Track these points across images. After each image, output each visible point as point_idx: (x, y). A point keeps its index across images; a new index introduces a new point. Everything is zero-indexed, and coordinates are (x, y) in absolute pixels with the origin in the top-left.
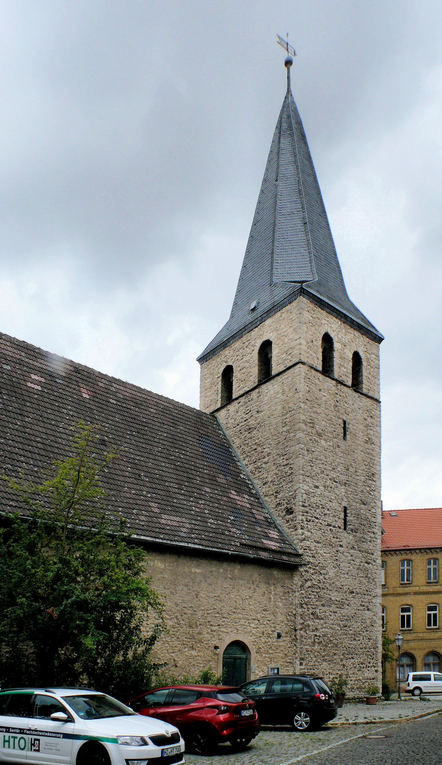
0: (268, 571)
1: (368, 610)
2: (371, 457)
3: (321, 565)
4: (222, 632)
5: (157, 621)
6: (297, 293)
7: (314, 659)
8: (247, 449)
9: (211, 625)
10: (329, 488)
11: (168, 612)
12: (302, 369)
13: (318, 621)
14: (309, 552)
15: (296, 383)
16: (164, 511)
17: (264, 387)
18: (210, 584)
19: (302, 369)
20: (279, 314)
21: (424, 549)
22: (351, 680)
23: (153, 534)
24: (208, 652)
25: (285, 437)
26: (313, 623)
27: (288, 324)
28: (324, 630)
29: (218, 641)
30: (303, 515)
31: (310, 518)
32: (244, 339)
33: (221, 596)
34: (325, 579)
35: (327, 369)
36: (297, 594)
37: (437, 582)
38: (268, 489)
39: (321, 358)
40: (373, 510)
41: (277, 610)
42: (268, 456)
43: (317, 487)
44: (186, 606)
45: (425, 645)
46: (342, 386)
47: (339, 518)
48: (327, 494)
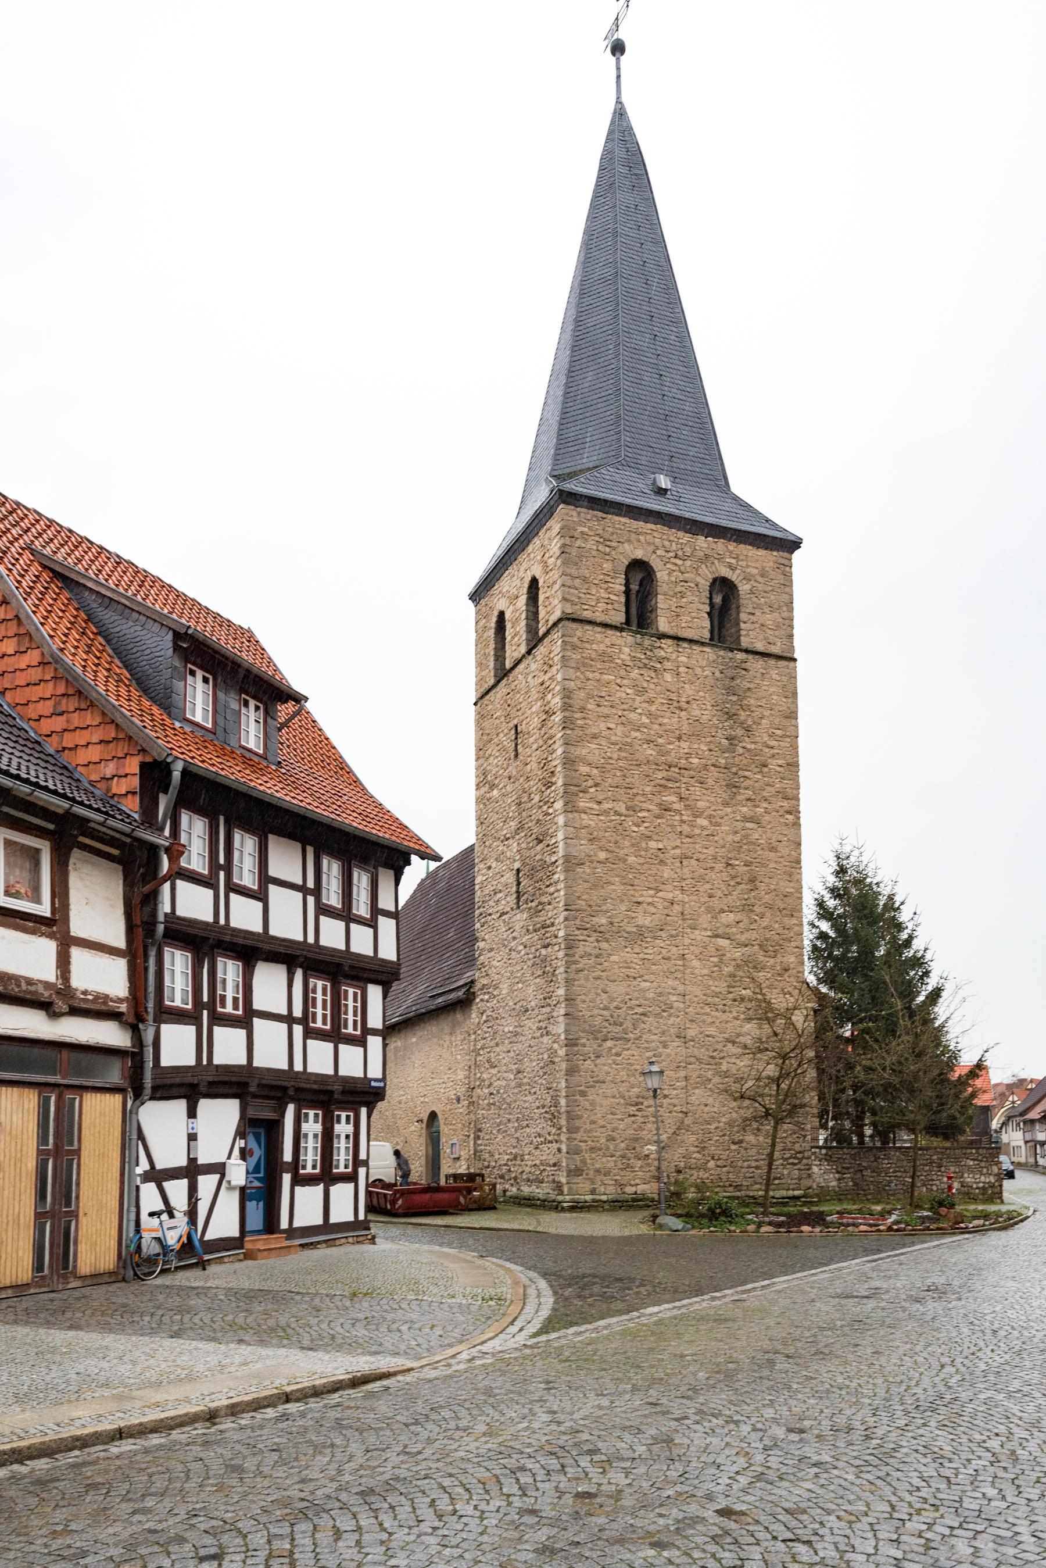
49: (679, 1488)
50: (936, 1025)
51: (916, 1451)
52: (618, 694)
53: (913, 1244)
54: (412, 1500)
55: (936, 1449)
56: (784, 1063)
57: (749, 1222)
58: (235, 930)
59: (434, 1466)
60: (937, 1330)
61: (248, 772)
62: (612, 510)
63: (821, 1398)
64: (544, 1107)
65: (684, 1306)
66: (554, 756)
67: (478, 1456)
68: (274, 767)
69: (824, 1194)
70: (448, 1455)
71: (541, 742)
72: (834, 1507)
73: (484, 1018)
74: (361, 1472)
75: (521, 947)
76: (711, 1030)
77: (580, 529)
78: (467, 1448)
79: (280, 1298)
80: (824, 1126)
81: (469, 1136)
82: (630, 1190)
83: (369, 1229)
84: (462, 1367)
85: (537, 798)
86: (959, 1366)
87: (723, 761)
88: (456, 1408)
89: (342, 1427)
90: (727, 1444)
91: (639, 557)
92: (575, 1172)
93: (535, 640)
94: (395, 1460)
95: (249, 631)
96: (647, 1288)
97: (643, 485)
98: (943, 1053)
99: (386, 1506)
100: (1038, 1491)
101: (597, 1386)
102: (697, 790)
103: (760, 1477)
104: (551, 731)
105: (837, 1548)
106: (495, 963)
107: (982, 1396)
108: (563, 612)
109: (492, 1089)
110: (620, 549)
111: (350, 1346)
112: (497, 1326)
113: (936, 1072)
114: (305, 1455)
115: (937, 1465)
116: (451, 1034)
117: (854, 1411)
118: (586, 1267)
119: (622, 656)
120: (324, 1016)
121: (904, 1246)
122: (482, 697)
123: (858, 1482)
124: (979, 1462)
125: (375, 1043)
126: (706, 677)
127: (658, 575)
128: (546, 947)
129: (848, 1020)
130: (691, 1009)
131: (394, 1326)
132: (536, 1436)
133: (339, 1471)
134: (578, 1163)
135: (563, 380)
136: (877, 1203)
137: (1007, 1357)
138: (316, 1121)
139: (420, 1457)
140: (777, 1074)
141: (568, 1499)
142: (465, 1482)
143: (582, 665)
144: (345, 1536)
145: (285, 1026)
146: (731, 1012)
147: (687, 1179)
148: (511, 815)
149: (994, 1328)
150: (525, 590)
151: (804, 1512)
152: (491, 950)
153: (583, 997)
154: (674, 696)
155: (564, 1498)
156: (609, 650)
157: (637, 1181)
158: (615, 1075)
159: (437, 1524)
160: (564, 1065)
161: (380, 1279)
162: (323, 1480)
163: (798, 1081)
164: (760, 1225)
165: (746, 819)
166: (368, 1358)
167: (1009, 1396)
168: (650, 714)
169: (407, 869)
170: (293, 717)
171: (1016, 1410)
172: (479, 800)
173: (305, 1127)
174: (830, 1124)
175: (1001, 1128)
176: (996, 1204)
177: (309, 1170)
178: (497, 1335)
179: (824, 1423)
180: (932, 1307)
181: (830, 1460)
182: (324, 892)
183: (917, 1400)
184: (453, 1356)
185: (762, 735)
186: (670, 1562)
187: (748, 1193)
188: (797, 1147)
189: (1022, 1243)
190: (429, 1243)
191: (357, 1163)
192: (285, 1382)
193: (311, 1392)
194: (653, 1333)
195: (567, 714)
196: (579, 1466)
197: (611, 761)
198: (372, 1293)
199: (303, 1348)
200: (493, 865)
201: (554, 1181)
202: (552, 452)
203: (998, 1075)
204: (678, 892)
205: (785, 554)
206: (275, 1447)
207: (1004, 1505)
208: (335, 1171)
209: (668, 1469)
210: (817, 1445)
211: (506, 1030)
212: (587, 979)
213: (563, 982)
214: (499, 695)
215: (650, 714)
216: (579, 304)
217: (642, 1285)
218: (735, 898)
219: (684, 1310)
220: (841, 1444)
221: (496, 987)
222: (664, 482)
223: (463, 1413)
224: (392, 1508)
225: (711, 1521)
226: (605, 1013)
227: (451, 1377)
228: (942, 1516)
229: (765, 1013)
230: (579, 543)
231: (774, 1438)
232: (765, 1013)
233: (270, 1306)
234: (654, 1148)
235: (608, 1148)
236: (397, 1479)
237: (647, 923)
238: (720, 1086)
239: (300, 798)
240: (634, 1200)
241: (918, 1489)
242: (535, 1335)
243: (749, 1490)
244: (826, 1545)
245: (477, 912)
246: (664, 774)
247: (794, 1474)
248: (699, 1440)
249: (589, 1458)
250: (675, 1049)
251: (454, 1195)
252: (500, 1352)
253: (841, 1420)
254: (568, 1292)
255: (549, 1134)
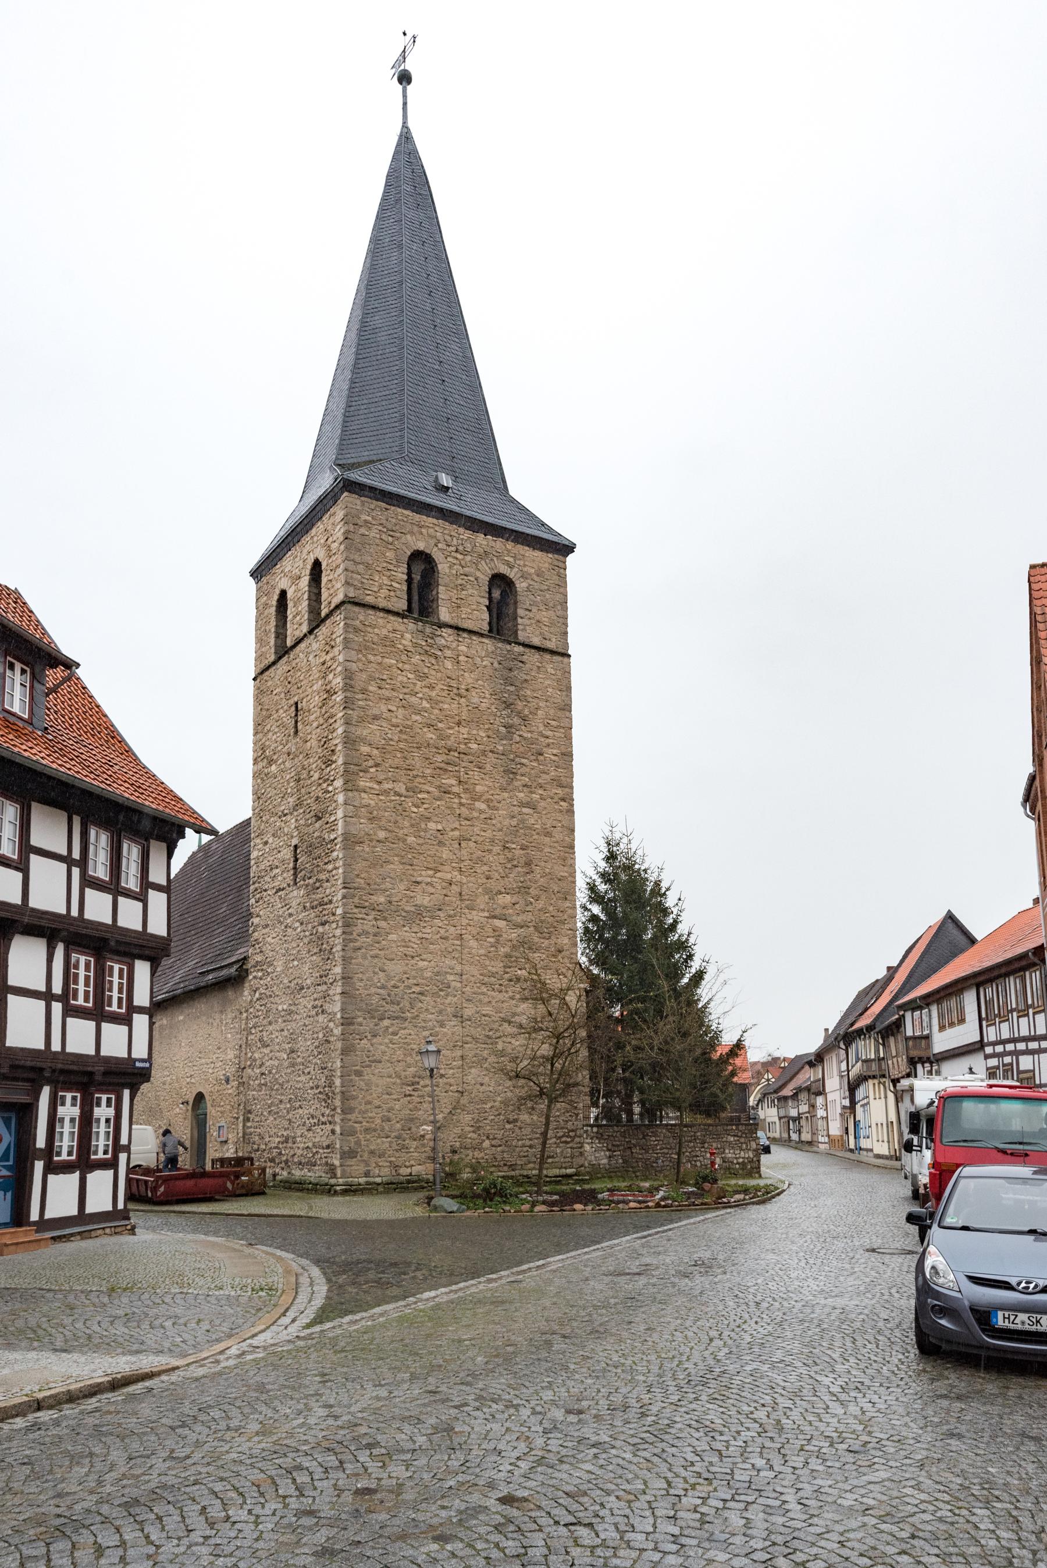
49: (461, 1478)
50: (700, 1006)
51: (689, 1426)
52: (400, 678)
53: (680, 1220)
54: (181, 1509)
55: (708, 1423)
56: (558, 1042)
57: (524, 1202)
58: (33, 910)
59: (204, 1470)
60: (705, 1304)
61: (11, 737)
63: (598, 1377)
64: (317, 1087)
65: (461, 1289)
66: (335, 735)
67: (251, 1457)
68: (40, 733)
69: (595, 1173)
70: (219, 1458)
71: (321, 721)
72: (614, 1487)
73: (257, 995)
74: (125, 1482)
75: (297, 924)
76: (487, 1010)
77: (364, 517)
78: (240, 1449)
79: (29, 1296)
80: (595, 1104)
81: (237, 1119)
82: (405, 1171)
83: (129, 1219)
84: (231, 1362)
85: (316, 776)
86: (726, 1338)
87: (501, 748)
88: (226, 1407)
89: (102, 1434)
90: (508, 1429)
91: (422, 548)
92: (349, 1154)
93: (317, 621)
94: (161, 1466)
95: (16, 591)
96: (424, 1272)
97: (427, 482)
98: (706, 1033)
99: (153, 1517)
100: (802, 1459)
101: (374, 1377)
102: (476, 775)
103: (541, 1461)
104: (331, 710)
105: (617, 1528)
106: (269, 939)
107: (748, 1368)
108: (346, 596)
109: (263, 1069)
110: (403, 540)
111: (109, 1346)
112: (268, 1319)
113: (699, 1051)
114: (61, 1467)
115: (709, 1439)
116: (221, 1012)
117: (629, 1388)
118: (361, 1252)
119: (404, 642)
120: (87, 993)
121: (672, 1222)
122: (262, 673)
123: (635, 1460)
124: (748, 1433)
125: (141, 1022)
126: (485, 667)
127: (440, 567)
128: (323, 924)
129: (619, 1000)
130: (468, 988)
131: (157, 1323)
132: (313, 1432)
133: (100, 1483)
134: (352, 1145)
135: (348, 375)
136: (646, 1180)
137: (770, 1328)
138: (74, 1105)
139: (189, 1461)
140: (551, 1053)
141: (347, 1497)
142: (238, 1485)
143: (365, 648)
144: (108, 1552)
145: (42, 1004)
146: (507, 992)
147: (462, 1159)
148: (289, 790)
149: (757, 1300)
150: (308, 572)
151: (585, 1494)
152: (267, 926)
153: (360, 975)
154: (454, 684)
155: (343, 1495)
156: (391, 635)
157: (412, 1162)
158: (391, 1054)
159: (208, 1533)
160: (339, 1045)
161: (142, 1272)
162: (81, 1493)
163: (572, 1060)
164: (534, 1204)
165: (522, 805)
166: (129, 1358)
167: (773, 1367)
168: (430, 699)
169: (181, 842)
170: (62, 683)
171: (779, 1379)
172: (256, 775)
173: (61, 1111)
174: (602, 1101)
175: (757, 1105)
176: (755, 1178)
177: (64, 1156)
178: (268, 1328)
179: (601, 1402)
180: (699, 1281)
181: (608, 1439)
182: (91, 863)
183: (689, 1375)
184: (222, 1352)
185: (537, 724)
186: (454, 1555)
187: (522, 1172)
188: (569, 1125)
189: (779, 1216)
190: (195, 1231)
191: (117, 1148)
192: (36, 1388)
193: (81, 1395)
194: (430, 1319)
195: (348, 694)
196: (358, 1461)
197: (391, 743)
198: (132, 1288)
199: (56, 1350)
200: (270, 841)
201: (327, 1163)
202: (337, 441)
203: (755, 1054)
204: (456, 873)
205: (561, 558)
206: (26, 1460)
207: (772, 1474)
208: (93, 1157)
209: (449, 1459)
210: (595, 1425)
211: (280, 1008)
212: (365, 957)
213: (340, 960)
214: (279, 672)
215: (430, 699)
216: (364, 306)
217: (417, 1269)
218: (513, 880)
219: (460, 1294)
220: (618, 1423)
221: (270, 964)
222: (445, 480)
223: (234, 1412)
224: (160, 1518)
225: (494, 1510)
226: (382, 991)
227: (220, 1374)
228: (715, 1490)
229: (540, 993)
230: (363, 531)
231: (554, 1421)
232: (540, 993)
233: (18, 1305)
234: (430, 1128)
235: (383, 1130)
236: (164, 1487)
237: (425, 902)
238: (496, 1065)
239: (68, 766)
240: (409, 1182)
241: (692, 1464)
242: (308, 1326)
243: (531, 1476)
244: (607, 1526)
245: (252, 888)
246: (444, 757)
247: (573, 1456)
248: (479, 1427)
249: (368, 1452)
250: (452, 1028)
251: (220, 1181)
252: (272, 1345)
253: (617, 1399)
254: (342, 1279)
255: (323, 1115)
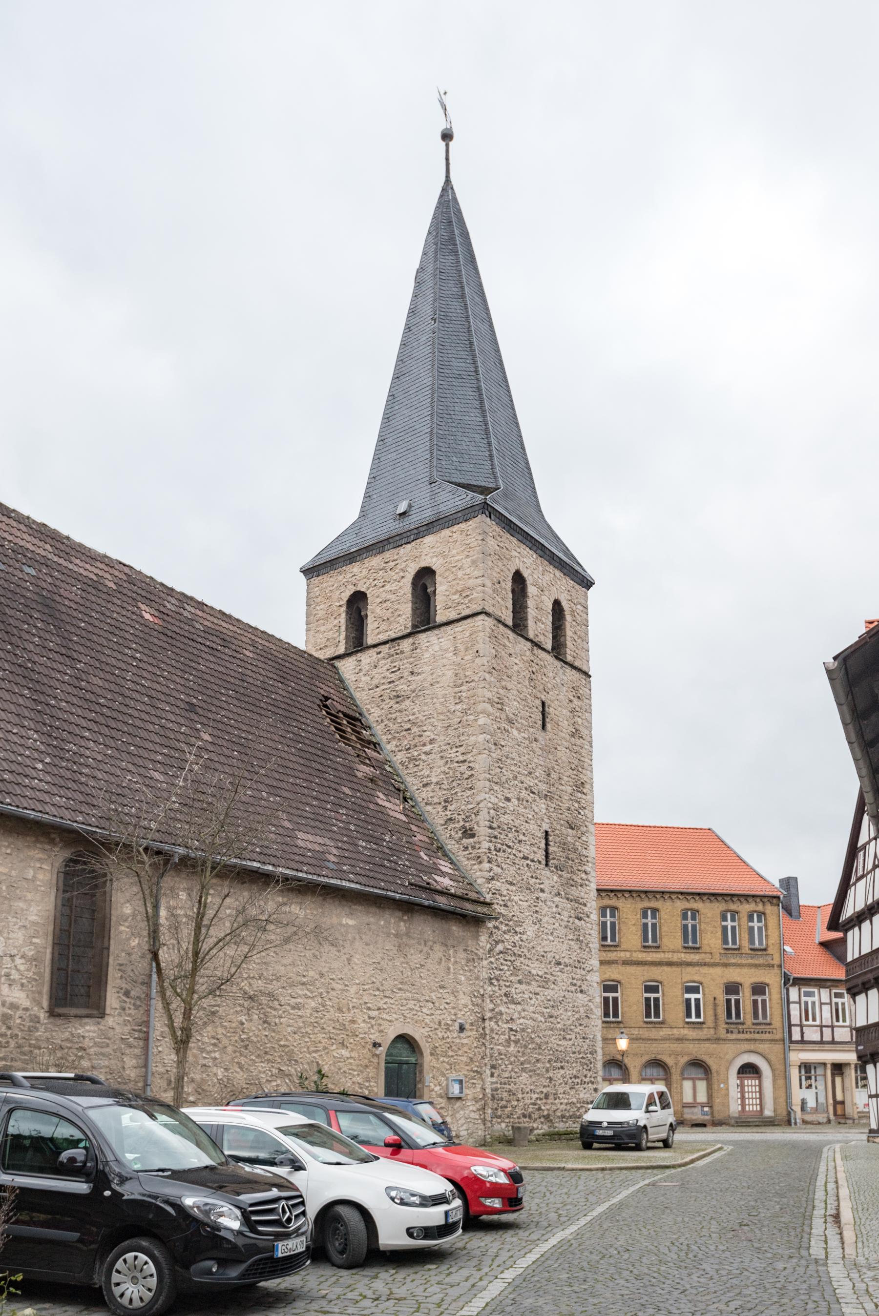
0: (446, 926)
1: (581, 991)
2: (579, 757)
3: (515, 919)
4: (384, 1020)
5: (293, 1000)
6: (477, 508)
7: (510, 1067)
8: (394, 727)
9: (369, 1009)
10: (525, 802)
11: (309, 987)
12: (486, 623)
13: (513, 1006)
14: (500, 898)
15: (478, 642)
16: (299, 827)
17: (422, 637)
18: (367, 944)
19: (486, 623)
20: (446, 532)
21: (637, 891)
22: (561, 1104)
23: (296, 866)
24: (364, 1052)
25: (459, 720)
26: (507, 1010)
27: (463, 551)
28: (522, 1021)
29: (377, 1034)
30: (491, 841)
31: (499, 846)
32: (387, 555)
33: (382, 963)
34: (522, 941)
35: (519, 626)
36: (485, 963)
37: (658, 947)
38: (432, 794)
39: (511, 607)
40: (584, 838)
41: (458, 986)
42: (431, 743)
43: (508, 799)
44: (334, 976)
45: (642, 1049)
46: (540, 651)
47: (539, 848)
48: (521, 810)
62: (528, 543)
